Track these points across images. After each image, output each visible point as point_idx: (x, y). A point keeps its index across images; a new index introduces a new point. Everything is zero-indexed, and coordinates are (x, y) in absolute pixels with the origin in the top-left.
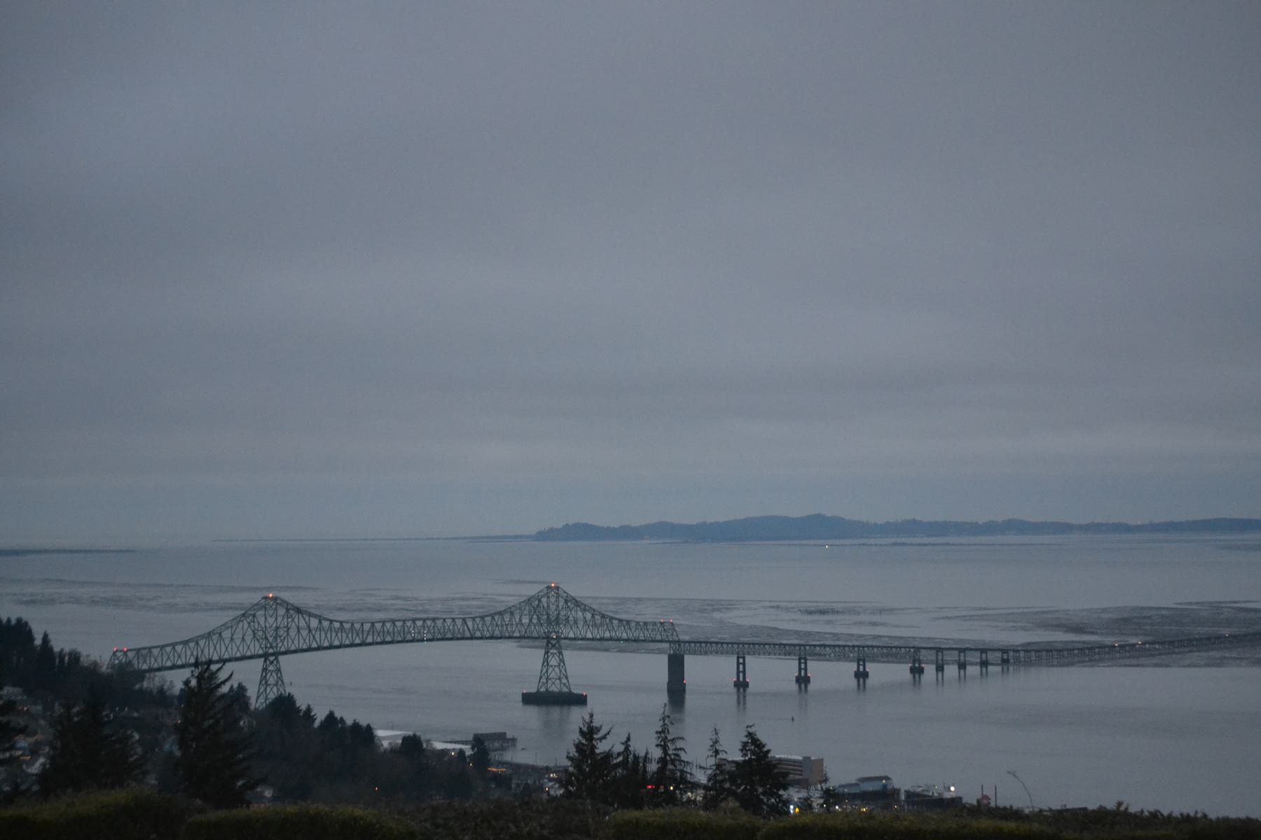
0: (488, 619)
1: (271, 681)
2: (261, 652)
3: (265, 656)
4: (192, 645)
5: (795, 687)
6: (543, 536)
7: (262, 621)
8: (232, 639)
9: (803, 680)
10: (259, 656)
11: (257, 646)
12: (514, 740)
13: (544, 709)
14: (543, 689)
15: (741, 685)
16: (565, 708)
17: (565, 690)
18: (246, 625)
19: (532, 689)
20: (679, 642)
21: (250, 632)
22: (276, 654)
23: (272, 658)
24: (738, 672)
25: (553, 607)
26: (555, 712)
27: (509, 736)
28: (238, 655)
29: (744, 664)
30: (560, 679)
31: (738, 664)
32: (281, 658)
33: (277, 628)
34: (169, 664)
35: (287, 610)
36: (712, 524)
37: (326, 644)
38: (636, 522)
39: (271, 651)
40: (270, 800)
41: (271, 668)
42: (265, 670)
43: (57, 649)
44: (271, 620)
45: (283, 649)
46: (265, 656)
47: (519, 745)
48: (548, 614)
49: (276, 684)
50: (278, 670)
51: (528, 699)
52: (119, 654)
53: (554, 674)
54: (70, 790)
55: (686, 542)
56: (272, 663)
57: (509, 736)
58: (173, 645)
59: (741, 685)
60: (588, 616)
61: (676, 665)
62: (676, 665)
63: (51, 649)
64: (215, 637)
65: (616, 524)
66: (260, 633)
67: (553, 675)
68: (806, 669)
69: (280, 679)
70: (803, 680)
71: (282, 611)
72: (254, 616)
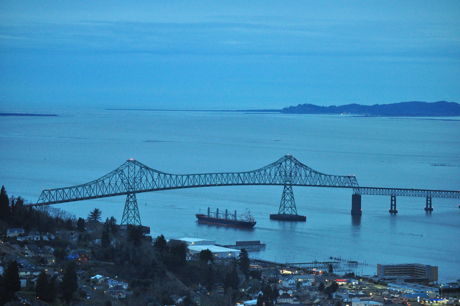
0: (252, 174)
1: (131, 207)
2: (126, 191)
3: (128, 193)
4: (87, 187)
5: (424, 212)
6: (287, 111)
7: (127, 174)
8: (110, 184)
9: (429, 209)
10: (125, 193)
11: (124, 187)
12: (264, 245)
13: (282, 223)
14: (282, 213)
15: (393, 212)
16: (294, 223)
17: (294, 213)
18: (118, 176)
19: (276, 212)
20: (358, 188)
21: (120, 180)
22: (134, 192)
23: (288, 187)
24: (392, 205)
25: (288, 168)
26: (288, 212)
27: (261, 243)
28: (113, 193)
29: (395, 200)
30: (291, 207)
31: (392, 200)
32: (137, 195)
33: (135, 178)
34: (74, 197)
35: (141, 168)
36: (381, 105)
37: (162, 187)
38: (338, 104)
39: (131, 190)
40: (128, 290)
41: (131, 200)
42: (128, 201)
43: (9, 197)
44: (132, 174)
45: (138, 190)
46: (128, 193)
47: (267, 247)
48: (285, 171)
49: (134, 209)
50: (135, 201)
51: (273, 217)
52: (46, 192)
53: (288, 204)
54: (25, 203)
55: (366, 116)
56: (131, 197)
57: (261, 243)
58: (321, 174)
59: (393, 212)
60: (308, 172)
61: (356, 200)
62: (356, 200)
63: (6, 197)
64: (100, 183)
65: (327, 105)
66: (126, 181)
67: (287, 205)
68: (431, 204)
69: (136, 206)
70: (429, 209)
71: (138, 168)
72: (122, 171)
